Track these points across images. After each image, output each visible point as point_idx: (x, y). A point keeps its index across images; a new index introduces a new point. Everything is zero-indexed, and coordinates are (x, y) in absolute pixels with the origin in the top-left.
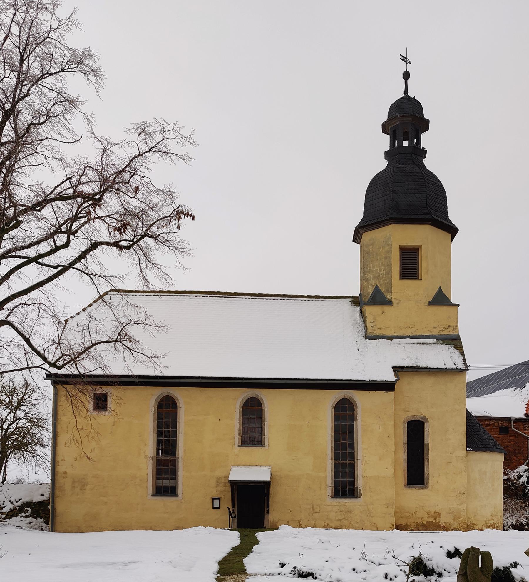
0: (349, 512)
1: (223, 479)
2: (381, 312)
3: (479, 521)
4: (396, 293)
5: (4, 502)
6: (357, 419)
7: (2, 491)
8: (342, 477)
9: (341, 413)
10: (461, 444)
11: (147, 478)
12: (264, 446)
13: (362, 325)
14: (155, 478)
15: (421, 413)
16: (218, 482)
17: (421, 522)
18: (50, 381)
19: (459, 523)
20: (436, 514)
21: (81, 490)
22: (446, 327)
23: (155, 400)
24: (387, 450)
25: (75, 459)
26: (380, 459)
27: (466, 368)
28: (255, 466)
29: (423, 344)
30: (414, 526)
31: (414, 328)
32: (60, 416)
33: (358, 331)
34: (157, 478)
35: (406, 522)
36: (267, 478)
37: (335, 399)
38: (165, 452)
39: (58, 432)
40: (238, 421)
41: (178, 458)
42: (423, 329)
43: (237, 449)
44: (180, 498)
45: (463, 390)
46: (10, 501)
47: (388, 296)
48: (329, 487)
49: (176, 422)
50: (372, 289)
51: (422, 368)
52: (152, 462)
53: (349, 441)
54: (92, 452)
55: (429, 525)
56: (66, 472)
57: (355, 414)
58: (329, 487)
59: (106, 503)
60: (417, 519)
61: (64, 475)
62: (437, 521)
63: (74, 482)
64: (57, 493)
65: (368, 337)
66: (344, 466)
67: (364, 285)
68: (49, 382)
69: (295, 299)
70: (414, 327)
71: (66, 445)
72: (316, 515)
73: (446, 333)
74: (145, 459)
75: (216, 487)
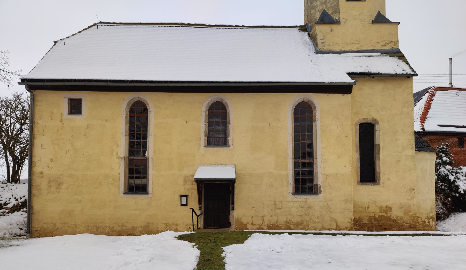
0: (310, 207)
1: (191, 177)
2: (330, 30)
3: (422, 214)
4: (343, 13)
5: (10, 199)
6: (315, 120)
7: (11, 190)
8: (302, 175)
9: (300, 115)
10: (410, 144)
11: (120, 177)
12: (229, 147)
13: (311, 44)
14: (127, 177)
15: (372, 116)
16: (185, 181)
17: (373, 215)
18: (24, 85)
19: (409, 217)
20: (387, 208)
21: (57, 189)
22: (388, 42)
23: (127, 104)
24: (345, 150)
25: (51, 160)
26: (339, 157)
27: (415, 73)
28: (220, 165)
29: (369, 56)
30: (367, 219)
31: (359, 43)
32: (37, 120)
33: (309, 48)
34: (130, 178)
36: (232, 176)
37: (295, 102)
39: (34, 135)
40: (204, 124)
41: (148, 158)
42: (367, 44)
43: (203, 150)
44: (150, 195)
45: (411, 95)
46: (15, 198)
47: (335, 17)
48: (291, 184)
49: (147, 125)
50: (319, 14)
51: (374, 74)
52: (124, 162)
53: (308, 142)
54: (67, 153)
55: (381, 219)
56: (42, 172)
57: (314, 115)
58: (291, 184)
59: (80, 201)
60: (370, 213)
61: (41, 175)
62: (389, 215)
63: (50, 182)
64: (34, 192)
67: (311, 12)
68: (23, 86)
69: (252, 28)
70: (359, 43)
71: (42, 147)
72: (278, 211)
73: (388, 47)
74: (117, 159)
75: (184, 185)
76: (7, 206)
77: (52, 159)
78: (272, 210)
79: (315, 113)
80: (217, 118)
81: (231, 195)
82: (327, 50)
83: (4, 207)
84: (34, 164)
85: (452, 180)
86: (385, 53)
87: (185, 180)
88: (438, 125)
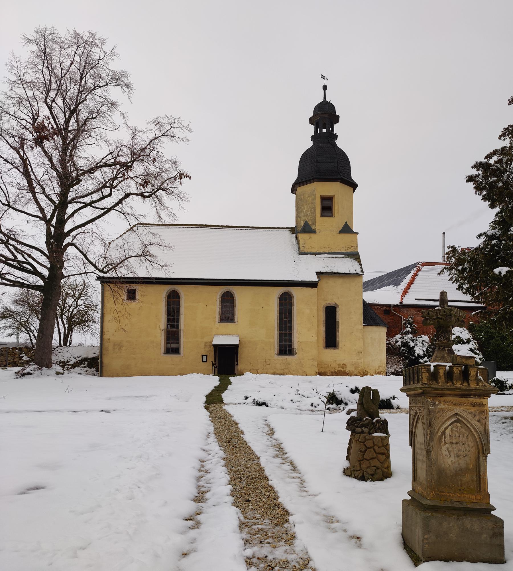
0: (289, 364)
1: (209, 343)
2: (309, 238)
6: (293, 306)
11: (161, 342)
12: (235, 322)
26: (308, 331)
34: (167, 343)
35: (325, 370)
36: (238, 343)
38: (172, 326)
42: (335, 248)
43: (217, 324)
44: (181, 355)
46: (74, 357)
47: (313, 227)
51: (335, 273)
53: (288, 319)
54: (126, 326)
59: (135, 358)
61: (108, 341)
63: (114, 345)
65: (300, 253)
66: (285, 335)
68: (99, 282)
69: (254, 229)
72: (267, 366)
73: (350, 251)
75: (205, 348)
76: (69, 363)
77: (116, 330)
78: (263, 366)
79: (293, 301)
80: (227, 303)
81: (236, 355)
82: (307, 251)
83: (67, 364)
84: (104, 334)
85: (411, 346)
86: (347, 255)
87: (205, 345)
88: (416, 299)
